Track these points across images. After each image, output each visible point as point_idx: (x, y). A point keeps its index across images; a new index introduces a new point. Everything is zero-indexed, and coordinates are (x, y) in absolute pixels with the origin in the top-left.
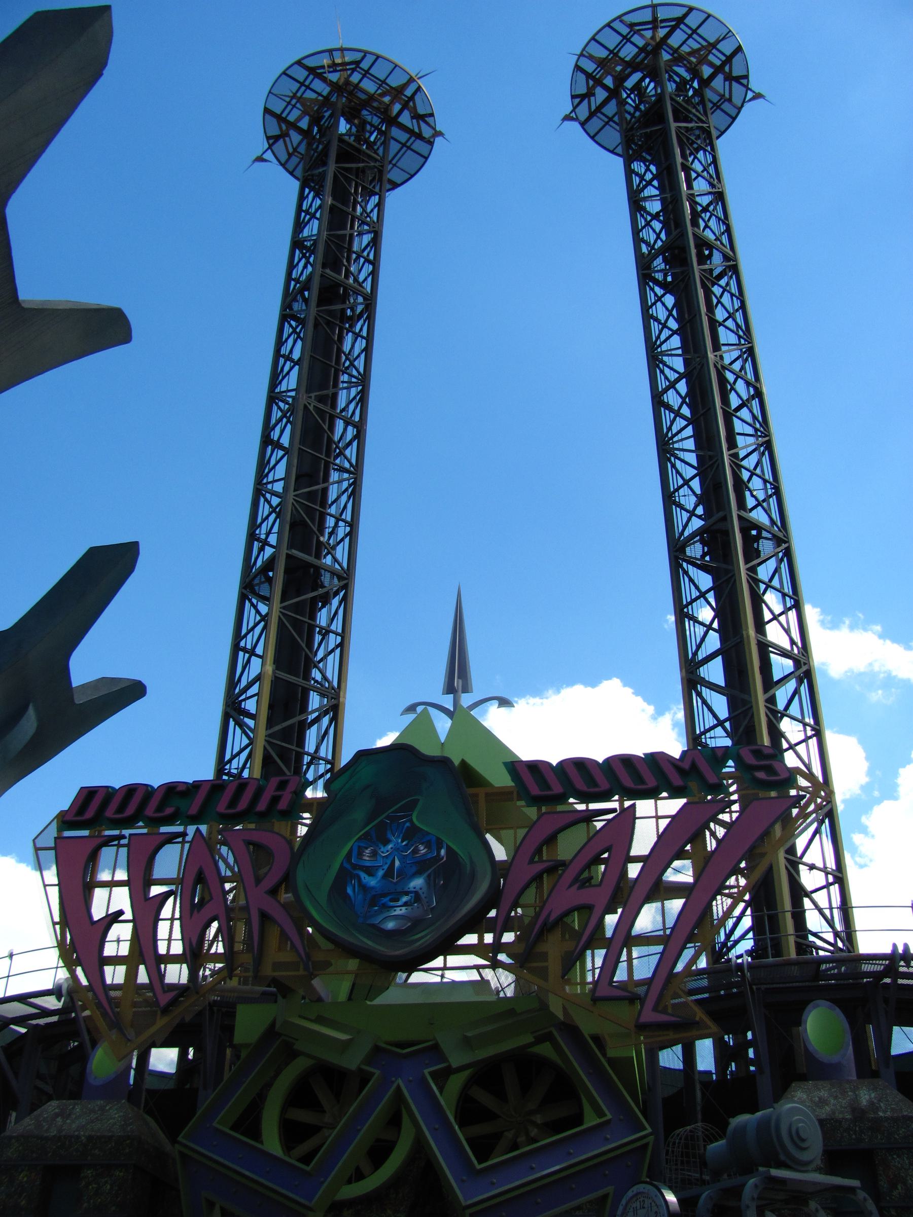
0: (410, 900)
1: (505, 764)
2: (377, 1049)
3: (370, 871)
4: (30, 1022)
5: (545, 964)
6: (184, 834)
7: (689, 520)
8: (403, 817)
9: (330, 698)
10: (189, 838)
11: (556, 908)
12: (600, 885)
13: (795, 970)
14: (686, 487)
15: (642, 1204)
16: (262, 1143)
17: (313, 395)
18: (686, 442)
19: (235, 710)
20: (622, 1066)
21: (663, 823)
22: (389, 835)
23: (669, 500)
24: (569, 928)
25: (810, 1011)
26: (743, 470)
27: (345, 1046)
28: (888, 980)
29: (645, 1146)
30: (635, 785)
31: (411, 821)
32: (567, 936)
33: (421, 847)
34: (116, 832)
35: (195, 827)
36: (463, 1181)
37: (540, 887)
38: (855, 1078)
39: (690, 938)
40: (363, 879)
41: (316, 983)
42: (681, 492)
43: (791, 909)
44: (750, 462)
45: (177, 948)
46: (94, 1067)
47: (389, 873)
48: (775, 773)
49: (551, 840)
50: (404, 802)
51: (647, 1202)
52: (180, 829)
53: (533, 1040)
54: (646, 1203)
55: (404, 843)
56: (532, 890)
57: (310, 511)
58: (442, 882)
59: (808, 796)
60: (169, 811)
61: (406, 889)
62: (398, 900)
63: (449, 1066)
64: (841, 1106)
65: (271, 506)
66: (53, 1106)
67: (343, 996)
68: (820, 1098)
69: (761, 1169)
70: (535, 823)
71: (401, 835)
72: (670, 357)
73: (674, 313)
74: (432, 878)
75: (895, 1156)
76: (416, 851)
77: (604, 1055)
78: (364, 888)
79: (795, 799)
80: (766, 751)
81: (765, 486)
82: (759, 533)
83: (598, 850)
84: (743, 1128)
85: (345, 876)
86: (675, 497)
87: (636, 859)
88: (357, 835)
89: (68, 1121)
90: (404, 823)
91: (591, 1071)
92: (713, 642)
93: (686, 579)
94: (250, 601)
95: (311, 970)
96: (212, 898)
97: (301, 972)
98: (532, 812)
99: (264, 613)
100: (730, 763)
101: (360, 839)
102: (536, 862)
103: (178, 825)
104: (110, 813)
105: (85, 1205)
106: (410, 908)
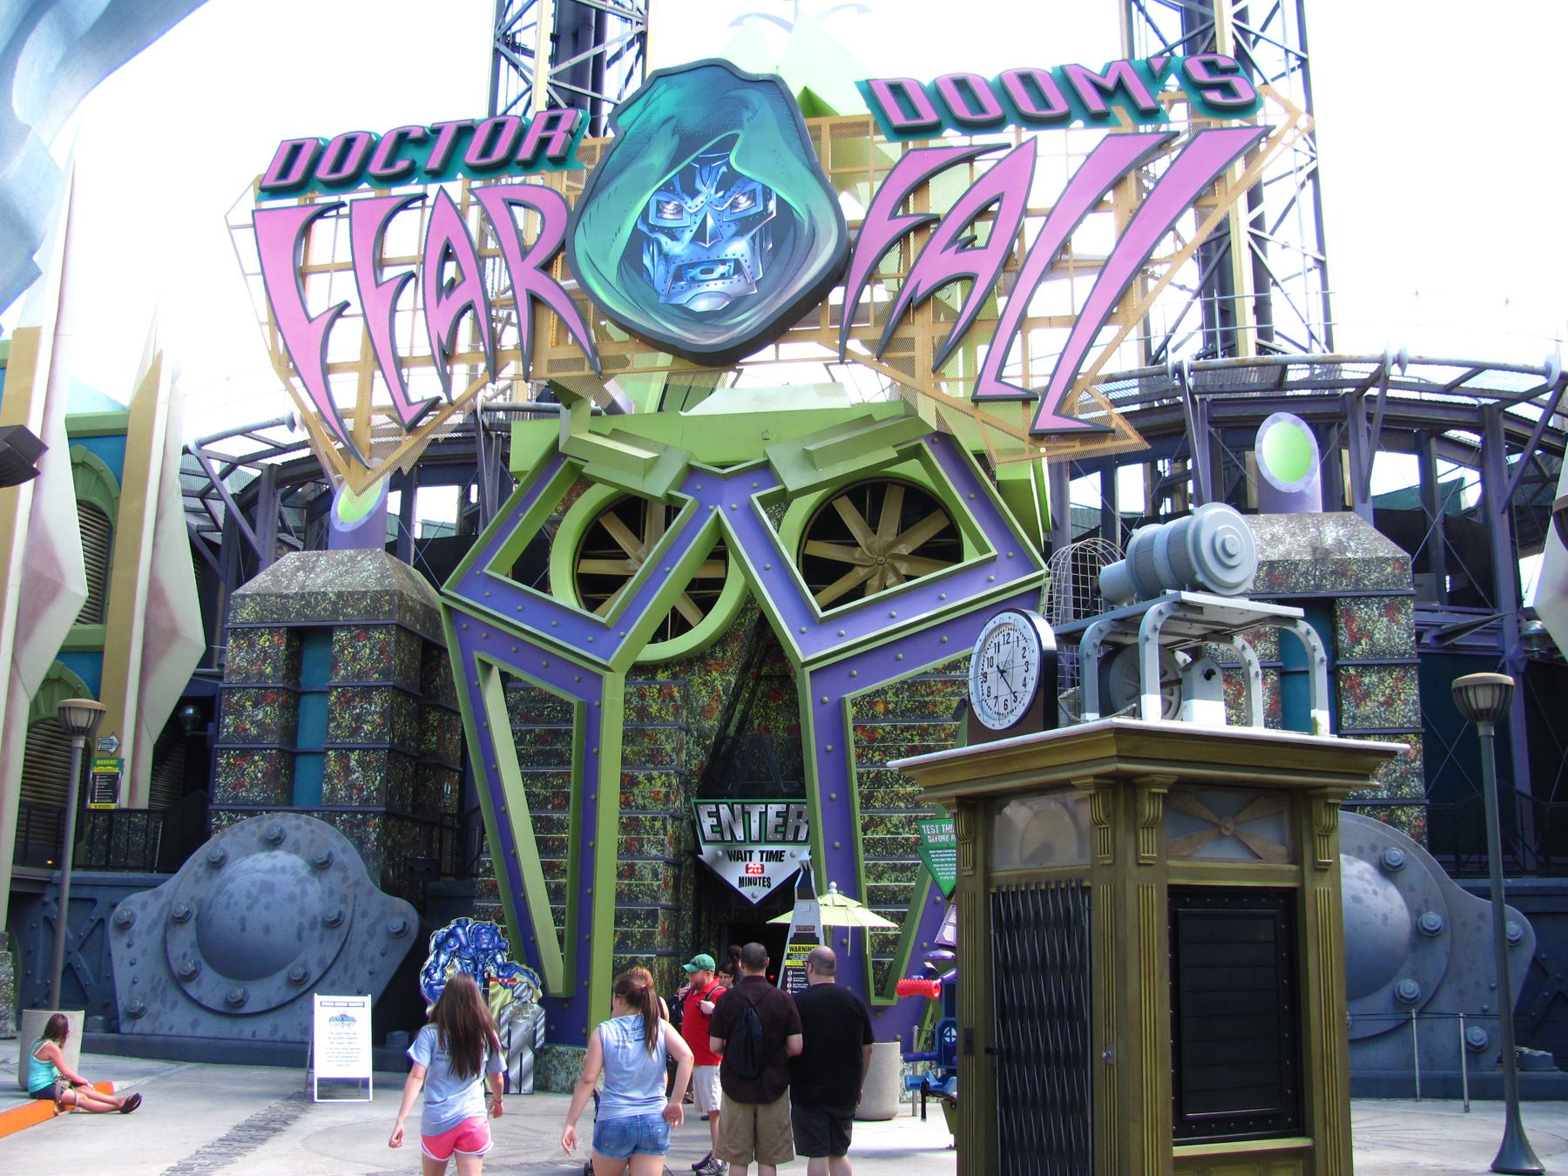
1: (858, 84)
2: (691, 471)
3: (673, 234)
6: (423, 197)
9: (634, 23)
12: (986, 247)
13: (1254, 378)
16: (551, 593)
19: (507, 45)
20: (1015, 492)
22: (699, 185)
24: (941, 307)
25: (1268, 427)
27: (649, 466)
28: (1373, 391)
29: (1039, 589)
31: (728, 164)
32: (942, 319)
33: (742, 199)
34: (333, 199)
36: (802, 632)
37: (905, 251)
38: (1320, 510)
39: (1107, 319)
41: (611, 387)
43: (1253, 293)
45: (423, 349)
46: (339, 512)
47: (700, 236)
49: (921, 186)
51: (1014, 635)
53: (897, 455)
56: (894, 255)
58: (771, 246)
60: (401, 165)
61: (723, 257)
62: (711, 271)
63: (785, 490)
64: (1299, 546)
66: (291, 559)
67: (651, 405)
68: (1273, 536)
69: (1169, 592)
71: (715, 184)
74: (757, 240)
75: (1362, 606)
76: (734, 205)
77: (992, 477)
78: (666, 257)
83: (986, 200)
84: (1150, 542)
85: (638, 243)
89: (312, 576)
90: (719, 167)
91: (972, 496)
95: (600, 369)
97: (587, 372)
98: (893, 150)
101: (659, 190)
104: (323, 173)
105: (343, 672)
106: (728, 281)
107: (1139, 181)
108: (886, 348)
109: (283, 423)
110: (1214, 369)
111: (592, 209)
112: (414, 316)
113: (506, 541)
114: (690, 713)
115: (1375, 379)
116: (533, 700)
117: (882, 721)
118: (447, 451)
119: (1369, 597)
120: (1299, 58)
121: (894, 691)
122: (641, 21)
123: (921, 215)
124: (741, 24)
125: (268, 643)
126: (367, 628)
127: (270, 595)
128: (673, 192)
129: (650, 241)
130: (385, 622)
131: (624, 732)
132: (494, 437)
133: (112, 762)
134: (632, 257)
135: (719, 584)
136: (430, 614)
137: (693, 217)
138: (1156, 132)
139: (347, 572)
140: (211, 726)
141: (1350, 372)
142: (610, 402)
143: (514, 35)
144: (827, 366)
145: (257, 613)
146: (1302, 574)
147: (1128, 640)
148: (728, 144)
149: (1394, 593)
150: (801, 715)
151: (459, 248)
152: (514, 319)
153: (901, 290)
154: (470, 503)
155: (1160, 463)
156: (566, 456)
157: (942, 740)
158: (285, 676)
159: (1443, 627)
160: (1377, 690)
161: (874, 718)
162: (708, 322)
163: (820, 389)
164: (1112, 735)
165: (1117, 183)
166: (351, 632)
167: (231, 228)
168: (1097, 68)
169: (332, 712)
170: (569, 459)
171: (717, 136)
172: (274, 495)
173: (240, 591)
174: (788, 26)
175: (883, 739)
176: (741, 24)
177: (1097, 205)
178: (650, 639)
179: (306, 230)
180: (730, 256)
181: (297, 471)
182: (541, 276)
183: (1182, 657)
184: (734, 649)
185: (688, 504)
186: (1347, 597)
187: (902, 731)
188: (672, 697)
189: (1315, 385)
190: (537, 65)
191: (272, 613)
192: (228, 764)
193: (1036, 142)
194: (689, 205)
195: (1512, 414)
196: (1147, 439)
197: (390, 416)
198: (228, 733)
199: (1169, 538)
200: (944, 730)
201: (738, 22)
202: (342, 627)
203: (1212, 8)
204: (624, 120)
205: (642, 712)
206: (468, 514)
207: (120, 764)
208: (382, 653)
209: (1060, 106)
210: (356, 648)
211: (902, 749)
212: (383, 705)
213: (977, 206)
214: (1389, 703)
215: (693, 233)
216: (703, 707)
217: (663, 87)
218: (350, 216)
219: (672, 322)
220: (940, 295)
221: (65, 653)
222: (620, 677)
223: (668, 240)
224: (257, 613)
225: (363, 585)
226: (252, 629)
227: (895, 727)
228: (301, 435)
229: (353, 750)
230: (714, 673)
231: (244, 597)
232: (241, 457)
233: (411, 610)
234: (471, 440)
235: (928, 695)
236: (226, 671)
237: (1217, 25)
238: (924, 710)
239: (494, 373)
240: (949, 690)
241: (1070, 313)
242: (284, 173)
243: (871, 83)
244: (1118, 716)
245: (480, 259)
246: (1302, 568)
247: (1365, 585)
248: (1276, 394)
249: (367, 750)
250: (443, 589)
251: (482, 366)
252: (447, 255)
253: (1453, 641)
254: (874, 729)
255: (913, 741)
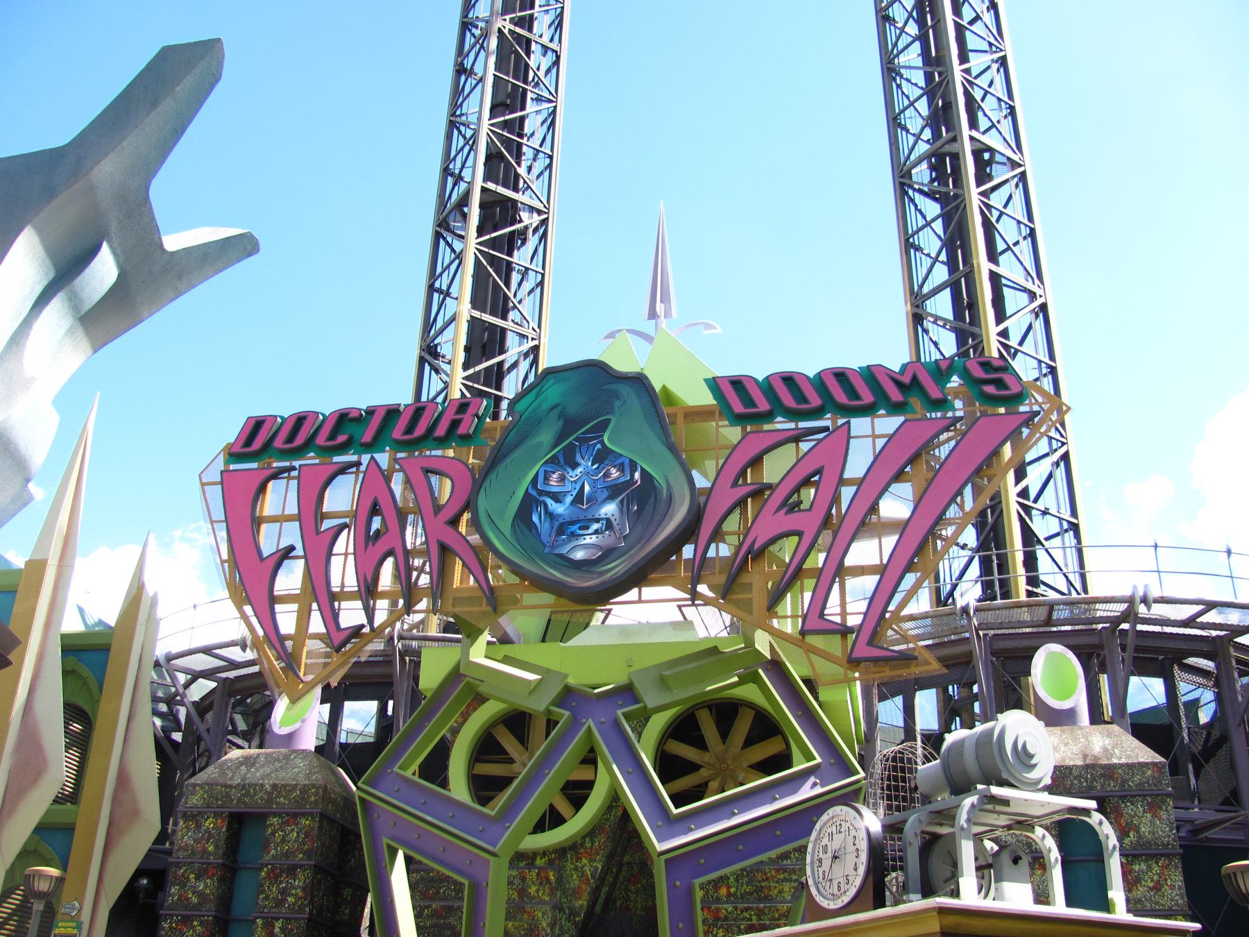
0: (601, 528)
1: (706, 381)
3: (557, 498)
4: (218, 675)
5: (749, 596)
6: (358, 464)
7: (915, 143)
8: (594, 438)
10: (363, 468)
11: (761, 535)
12: (810, 509)
13: (1025, 616)
14: (912, 107)
15: (838, 828)
16: (449, 790)
17: (508, 17)
18: (911, 57)
21: (880, 443)
22: (579, 459)
23: (895, 123)
26: (975, 86)
28: (1125, 626)
29: (860, 789)
30: (850, 401)
31: (602, 443)
33: (613, 471)
34: (287, 464)
35: (369, 456)
39: (909, 568)
40: (550, 505)
42: (907, 113)
44: (983, 81)
45: (352, 583)
47: (579, 499)
48: (1006, 387)
50: (594, 422)
51: (845, 826)
52: (354, 458)
54: (843, 826)
55: (595, 467)
57: (507, 142)
59: (1042, 413)
60: (341, 438)
62: (588, 528)
63: (645, 707)
64: (1072, 753)
65: (465, 137)
69: (980, 787)
70: (736, 446)
71: (592, 458)
72: (908, 70)
73: (914, 14)
74: (625, 502)
75: (1128, 804)
76: (607, 475)
77: (816, 698)
78: (551, 516)
79: (1028, 415)
80: (996, 364)
81: (1000, 106)
82: (992, 156)
84: (960, 744)
85: (529, 504)
86: (900, 119)
87: (850, 482)
88: (543, 458)
89: (253, 770)
90: (596, 444)
92: (941, 274)
93: (912, 207)
94: (445, 239)
96: (388, 531)
98: (733, 434)
99: (458, 251)
100: (955, 378)
102: (740, 485)
103: (353, 454)
105: (273, 852)
106: (600, 536)
107: (928, 463)
108: (728, 593)
109: (237, 645)
110: (995, 609)
111: (493, 476)
112: (346, 559)
113: (415, 744)
114: (563, 893)
115: (1125, 617)
116: (432, 880)
117: (726, 903)
118: (368, 671)
119: (1132, 796)
120: (1049, 366)
121: (735, 876)
122: (535, 337)
123: (759, 484)
124: (614, 337)
125: (212, 825)
126: (295, 815)
127: (217, 785)
128: (558, 463)
129: (538, 503)
130: (311, 810)
131: (507, 909)
132: (408, 661)
133: (74, 924)
134: (523, 515)
135: (590, 785)
136: (348, 802)
137: (574, 484)
138: (944, 417)
139: (281, 767)
140: (160, 895)
141: (1103, 611)
142: (502, 633)
143: (436, 346)
144: (680, 607)
145: (205, 799)
146: (1075, 778)
147: (944, 830)
148: (603, 426)
149: (1154, 792)
150: (657, 898)
151: (385, 505)
152: (427, 568)
153: (741, 545)
154: (387, 715)
155: (950, 688)
156: (465, 676)
157: (775, 919)
158: (224, 854)
159: (1196, 822)
160: (1146, 877)
161: (718, 900)
162: (585, 568)
163: (674, 625)
164: (936, 913)
165: (913, 460)
166: (283, 818)
167: (203, 485)
168: (896, 367)
169: (261, 885)
170: (467, 679)
171: (593, 420)
172: (227, 704)
173: (192, 780)
174: (648, 338)
175: (726, 919)
176: (614, 337)
177: (899, 477)
178: (531, 828)
179: (262, 489)
180: (603, 516)
181: (245, 684)
182: (449, 529)
183: (990, 845)
184: (600, 840)
185: (565, 718)
186: (1115, 796)
187: (742, 911)
188: (548, 880)
189: (1075, 622)
190: (452, 370)
191: (217, 799)
192: (171, 928)
193: (849, 426)
194: (570, 474)
195: (1240, 644)
196: (947, 666)
197: (325, 643)
198: (172, 900)
199: (977, 740)
200: (778, 910)
201: (611, 335)
202: (275, 814)
203: (980, 327)
204: (520, 407)
205: (523, 892)
206: (385, 724)
207: (79, 926)
208: (306, 836)
209: (867, 397)
210: (285, 832)
211: (742, 927)
212: (305, 881)
213: (802, 478)
214: (1157, 888)
215: (572, 497)
216: (574, 889)
217: (550, 383)
218: (298, 478)
219: (554, 568)
220: (772, 548)
221: (40, 829)
222: (505, 861)
223: (553, 503)
224: (205, 799)
225: (294, 779)
226: (200, 813)
227: (736, 908)
228: (250, 655)
229: (277, 919)
230: (584, 860)
231: (194, 785)
232: (202, 671)
233: (333, 801)
234: (390, 663)
235: (764, 881)
236: (176, 848)
237: (985, 342)
238: (761, 895)
239: (409, 609)
240: (782, 876)
241: (878, 562)
242: (249, 441)
243: (717, 380)
244: (939, 896)
245: (402, 516)
246: (1075, 772)
247: (1129, 785)
248: (1047, 629)
249: (290, 919)
250: (359, 784)
251: (401, 602)
252: (375, 510)
253: (1206, 834)
254: (718, 910)
255: (751, 920)
